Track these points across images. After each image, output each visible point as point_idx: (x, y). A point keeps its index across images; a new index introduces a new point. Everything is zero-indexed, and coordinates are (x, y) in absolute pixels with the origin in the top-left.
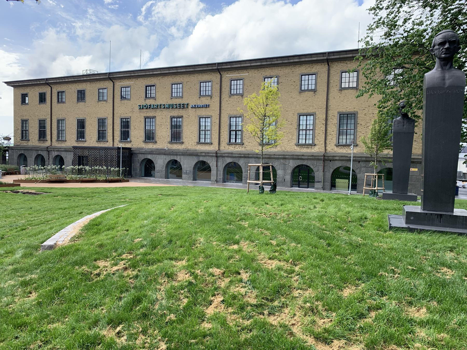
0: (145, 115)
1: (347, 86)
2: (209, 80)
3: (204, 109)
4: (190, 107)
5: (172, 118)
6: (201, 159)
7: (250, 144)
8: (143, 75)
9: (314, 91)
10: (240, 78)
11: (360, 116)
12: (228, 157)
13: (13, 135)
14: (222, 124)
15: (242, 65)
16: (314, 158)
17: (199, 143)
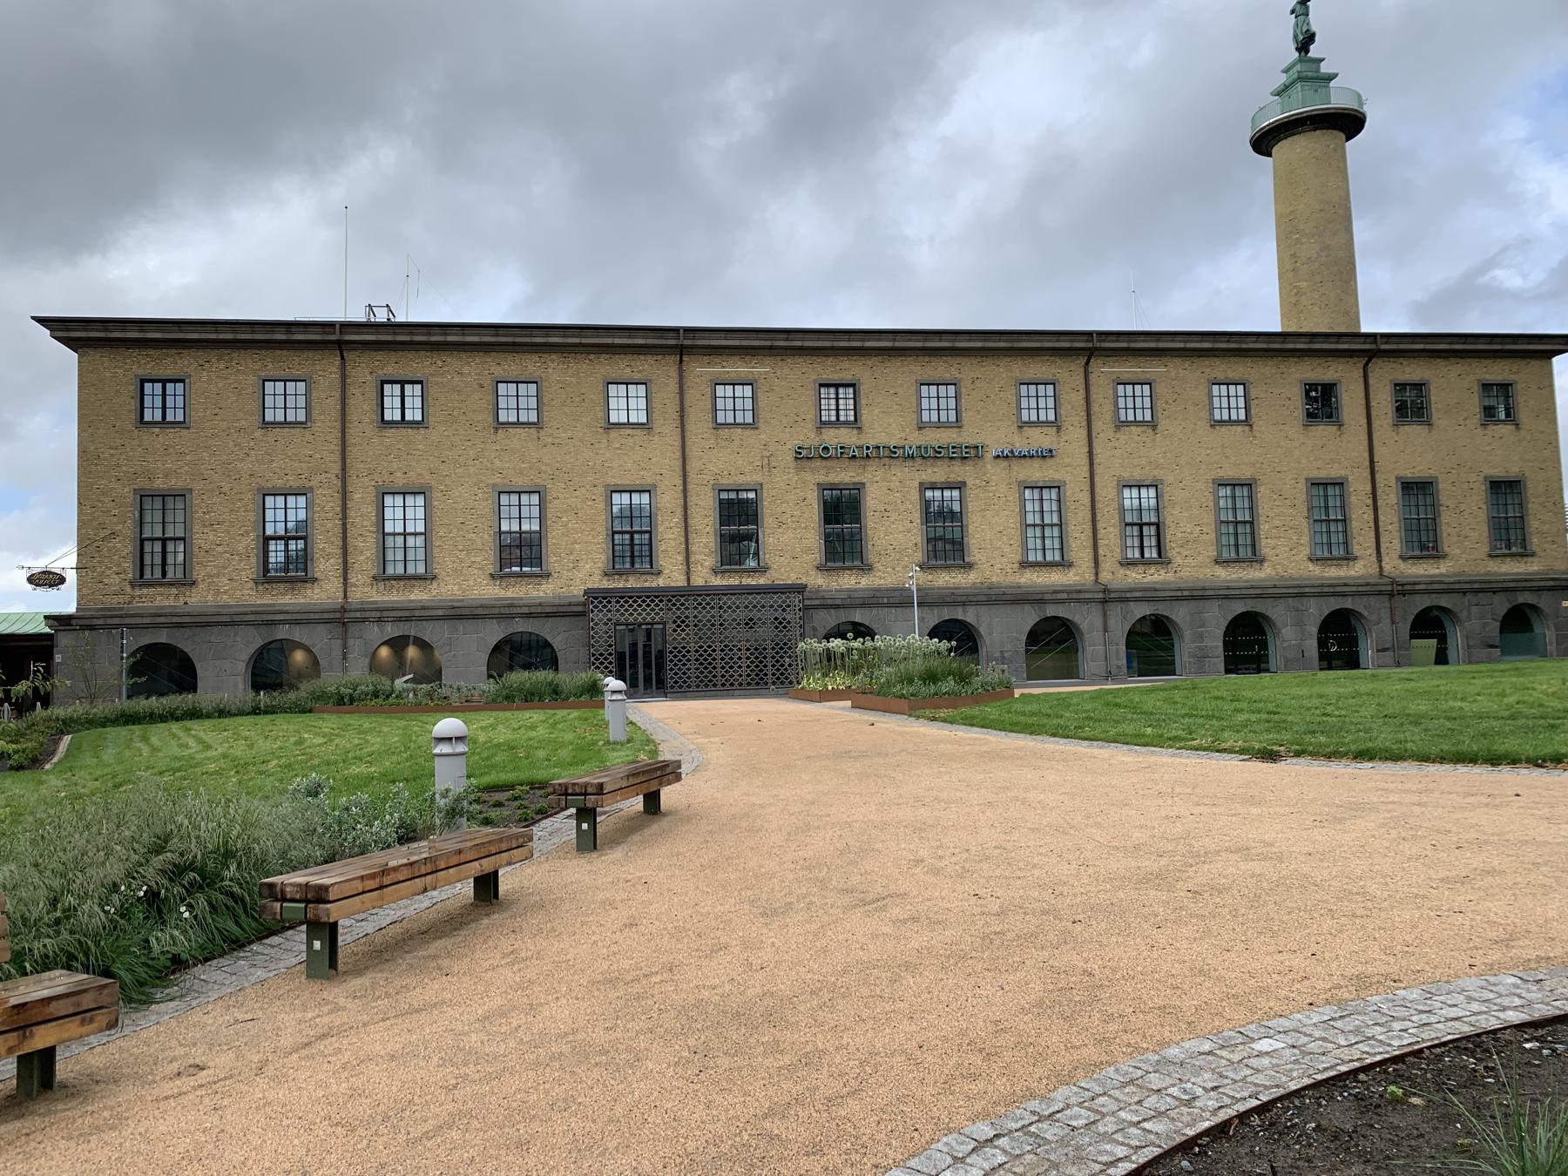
0: (821, 479)
1: (513, 419)
2: (1048, 377)
3: (1036, 463)
4: (989, 457)
5: (924, 487)
6: (1051, 611)
7: (1190, 560)
8: (506, 344)
9: (645, 427)
10: (1142, 378)
11: (1443, 486)
12: (1138, 600)
13: (72, 560)
14: (1099, 505)
15: (1161, 345)
16: (1074, 596)
17: (1025, 565)
